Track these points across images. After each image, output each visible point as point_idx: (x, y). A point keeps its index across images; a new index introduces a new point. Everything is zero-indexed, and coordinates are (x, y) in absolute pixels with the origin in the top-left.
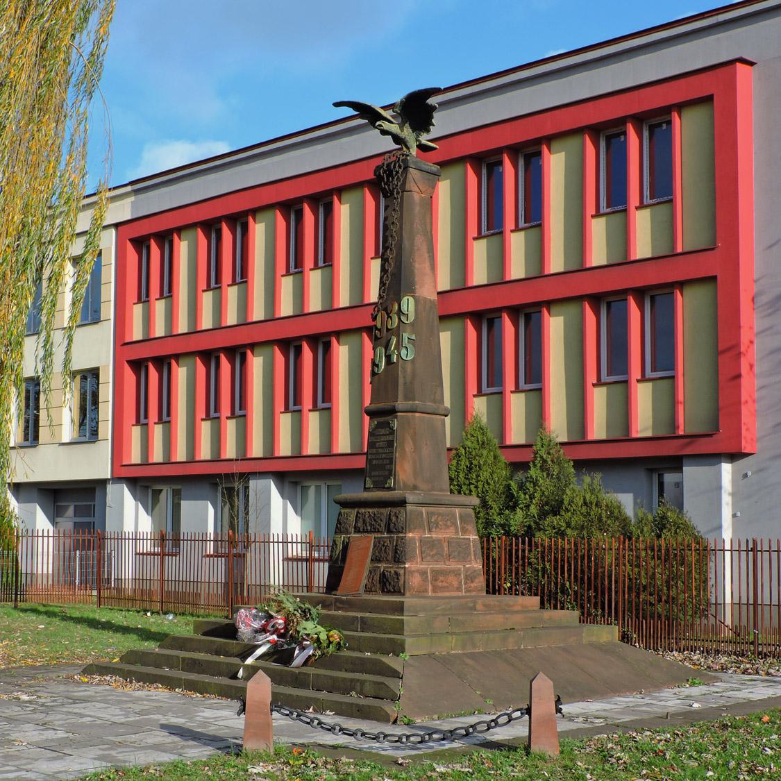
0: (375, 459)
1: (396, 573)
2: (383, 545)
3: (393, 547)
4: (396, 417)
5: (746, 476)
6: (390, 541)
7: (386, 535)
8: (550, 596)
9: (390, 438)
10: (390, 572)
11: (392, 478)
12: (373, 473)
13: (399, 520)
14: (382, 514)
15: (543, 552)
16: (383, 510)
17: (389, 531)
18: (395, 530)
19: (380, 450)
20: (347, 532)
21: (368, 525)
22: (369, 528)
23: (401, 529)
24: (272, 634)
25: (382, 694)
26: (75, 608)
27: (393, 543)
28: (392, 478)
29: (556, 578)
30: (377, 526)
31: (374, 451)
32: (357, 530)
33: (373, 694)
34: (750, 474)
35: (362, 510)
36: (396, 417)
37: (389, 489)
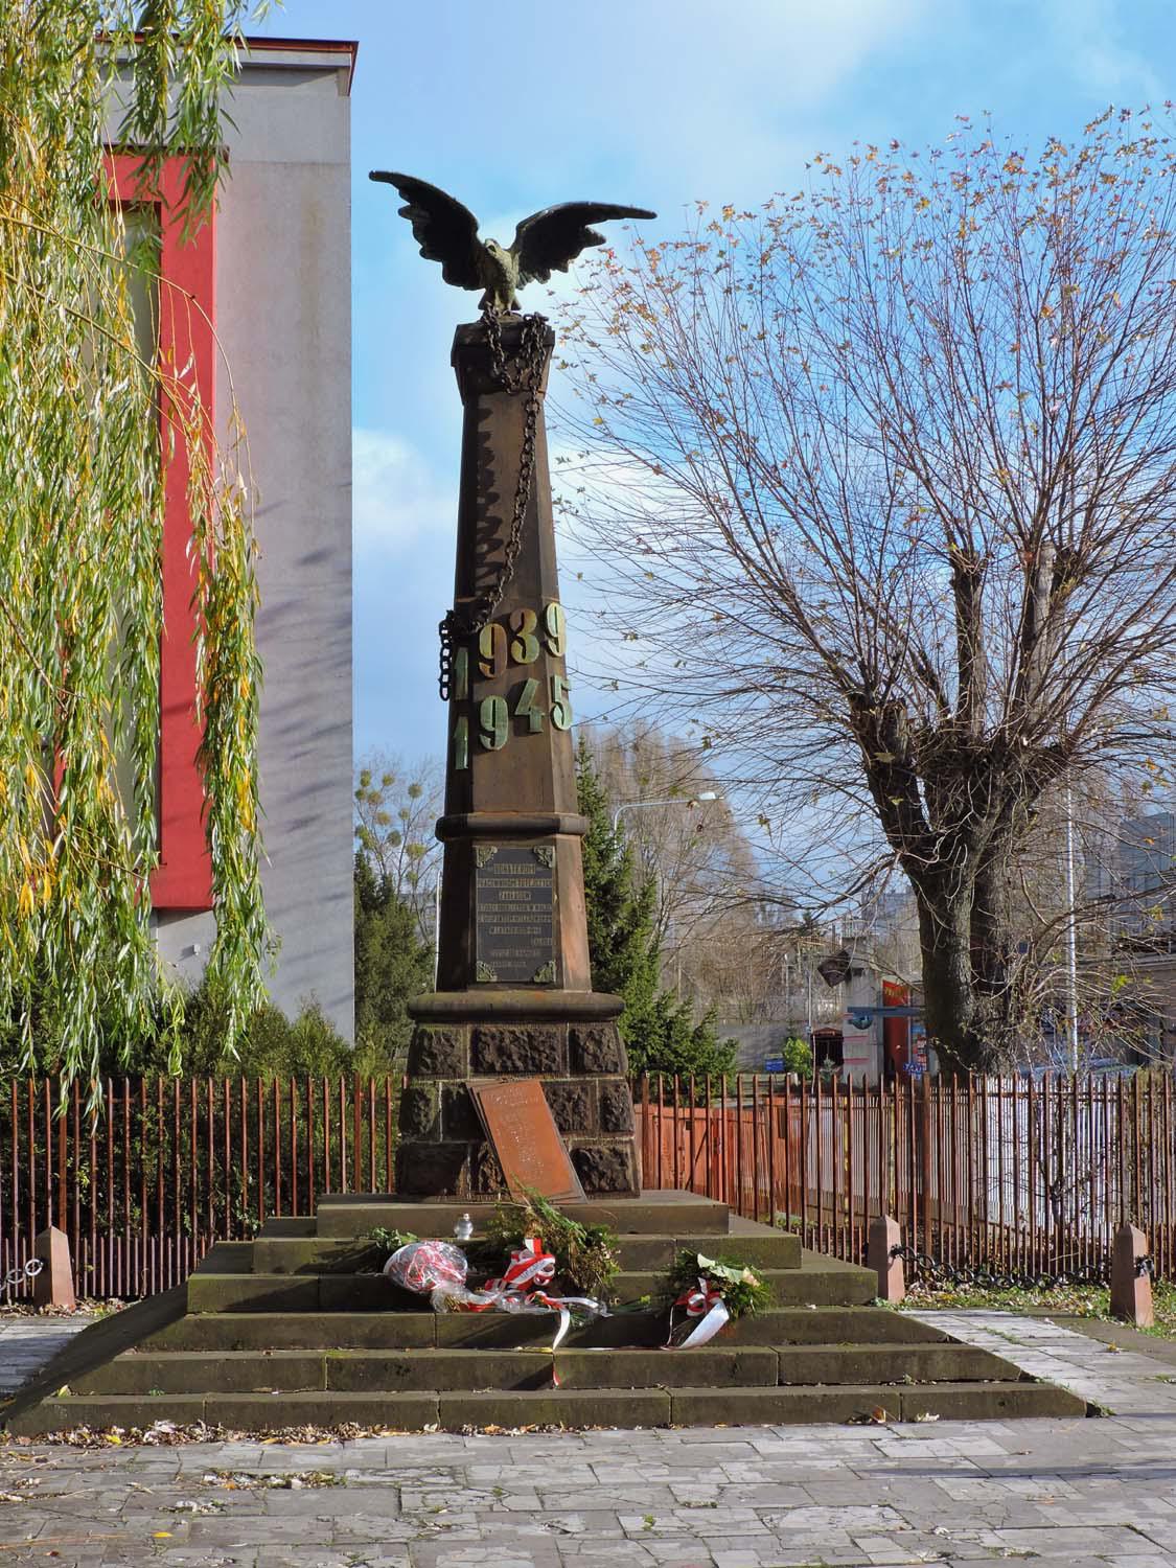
0: (497, 925)
1: (616, 1153)
2: (569, 1099)
3: (593, 1102)
4: (554, 843)
5: (190, 951)
6: (583, 1089)
7: (569, 1078)
8: (189, 1199)
9: (542, 883)
10: (599, 1152)
11: (553, 963)
12: (493, 953)
13: (605, 1049)
14: (550, 1036)
15: (169, 1111)
16: (552, 1029)
17: (578, 1067)
18: (595, 1068)
19: (512, 908)
20: (454, 1071)
21: (515, 1057)
22: (519, 1064)
23: (611, 1067)
24: (706, 1269)
25: (977, 1371)
26: (538, 1211)
27: (594, 1095)
28: (553, 963)
29: (205, 1161)
30: (545, 1061)
31: (496, 907)
32: (480, 1067)
33: (955, 1375)
34: (197, 949)
35: (488, 1028)
36: (554, 843)
37: (546, 985)
